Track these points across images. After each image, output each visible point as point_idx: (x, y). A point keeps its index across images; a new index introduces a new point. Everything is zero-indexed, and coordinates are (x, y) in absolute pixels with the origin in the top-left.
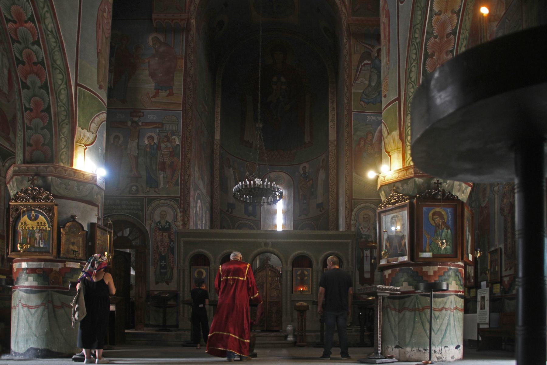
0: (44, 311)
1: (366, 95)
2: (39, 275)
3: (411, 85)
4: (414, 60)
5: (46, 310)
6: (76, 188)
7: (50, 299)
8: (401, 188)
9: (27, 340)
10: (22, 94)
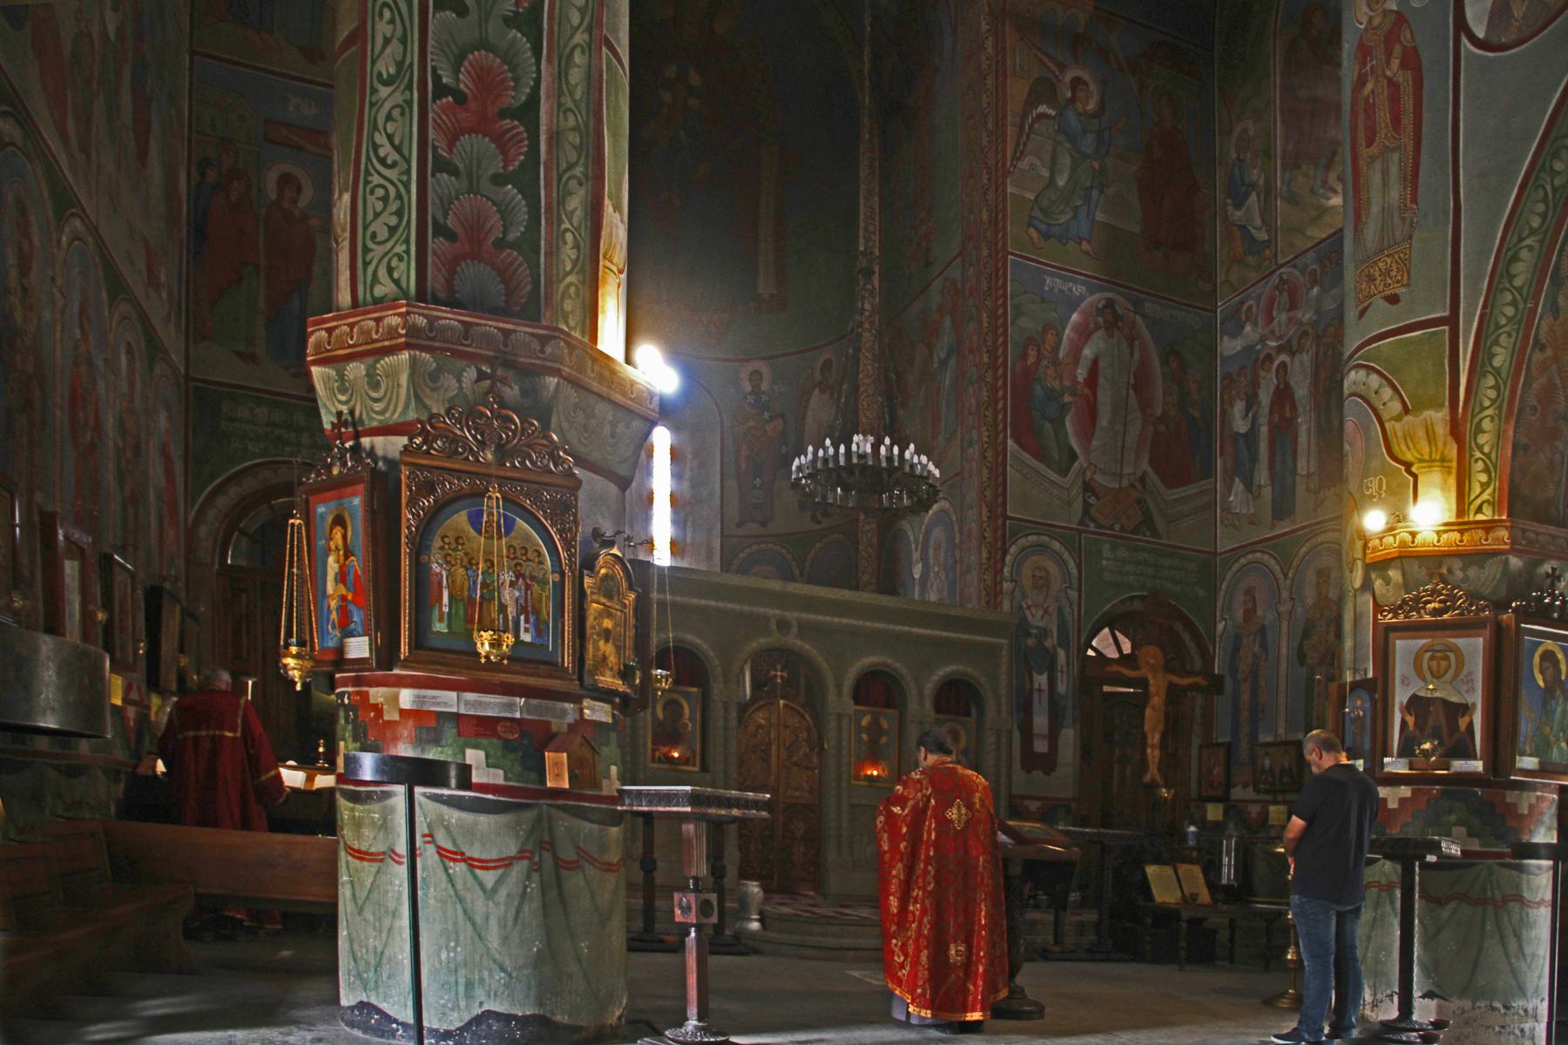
0: (528, 878)
1: (1042, 210)
2: (508, 746)
3: (1509, 297)
4: (1533, 232)
5: (536, 876)
6: (607, 428)
7: (546, 837)
8: (1459, 574)
9: (469, 985)
10: (431, 27)
